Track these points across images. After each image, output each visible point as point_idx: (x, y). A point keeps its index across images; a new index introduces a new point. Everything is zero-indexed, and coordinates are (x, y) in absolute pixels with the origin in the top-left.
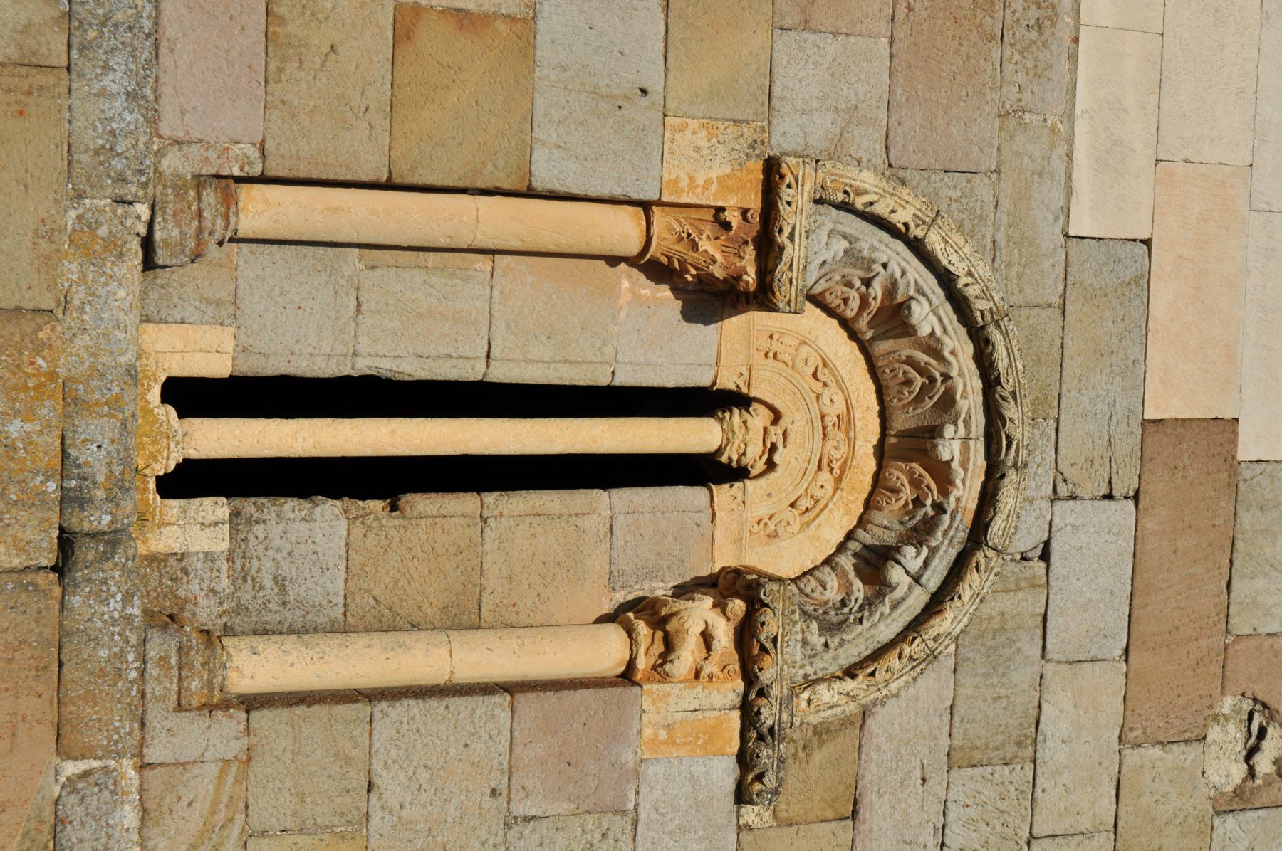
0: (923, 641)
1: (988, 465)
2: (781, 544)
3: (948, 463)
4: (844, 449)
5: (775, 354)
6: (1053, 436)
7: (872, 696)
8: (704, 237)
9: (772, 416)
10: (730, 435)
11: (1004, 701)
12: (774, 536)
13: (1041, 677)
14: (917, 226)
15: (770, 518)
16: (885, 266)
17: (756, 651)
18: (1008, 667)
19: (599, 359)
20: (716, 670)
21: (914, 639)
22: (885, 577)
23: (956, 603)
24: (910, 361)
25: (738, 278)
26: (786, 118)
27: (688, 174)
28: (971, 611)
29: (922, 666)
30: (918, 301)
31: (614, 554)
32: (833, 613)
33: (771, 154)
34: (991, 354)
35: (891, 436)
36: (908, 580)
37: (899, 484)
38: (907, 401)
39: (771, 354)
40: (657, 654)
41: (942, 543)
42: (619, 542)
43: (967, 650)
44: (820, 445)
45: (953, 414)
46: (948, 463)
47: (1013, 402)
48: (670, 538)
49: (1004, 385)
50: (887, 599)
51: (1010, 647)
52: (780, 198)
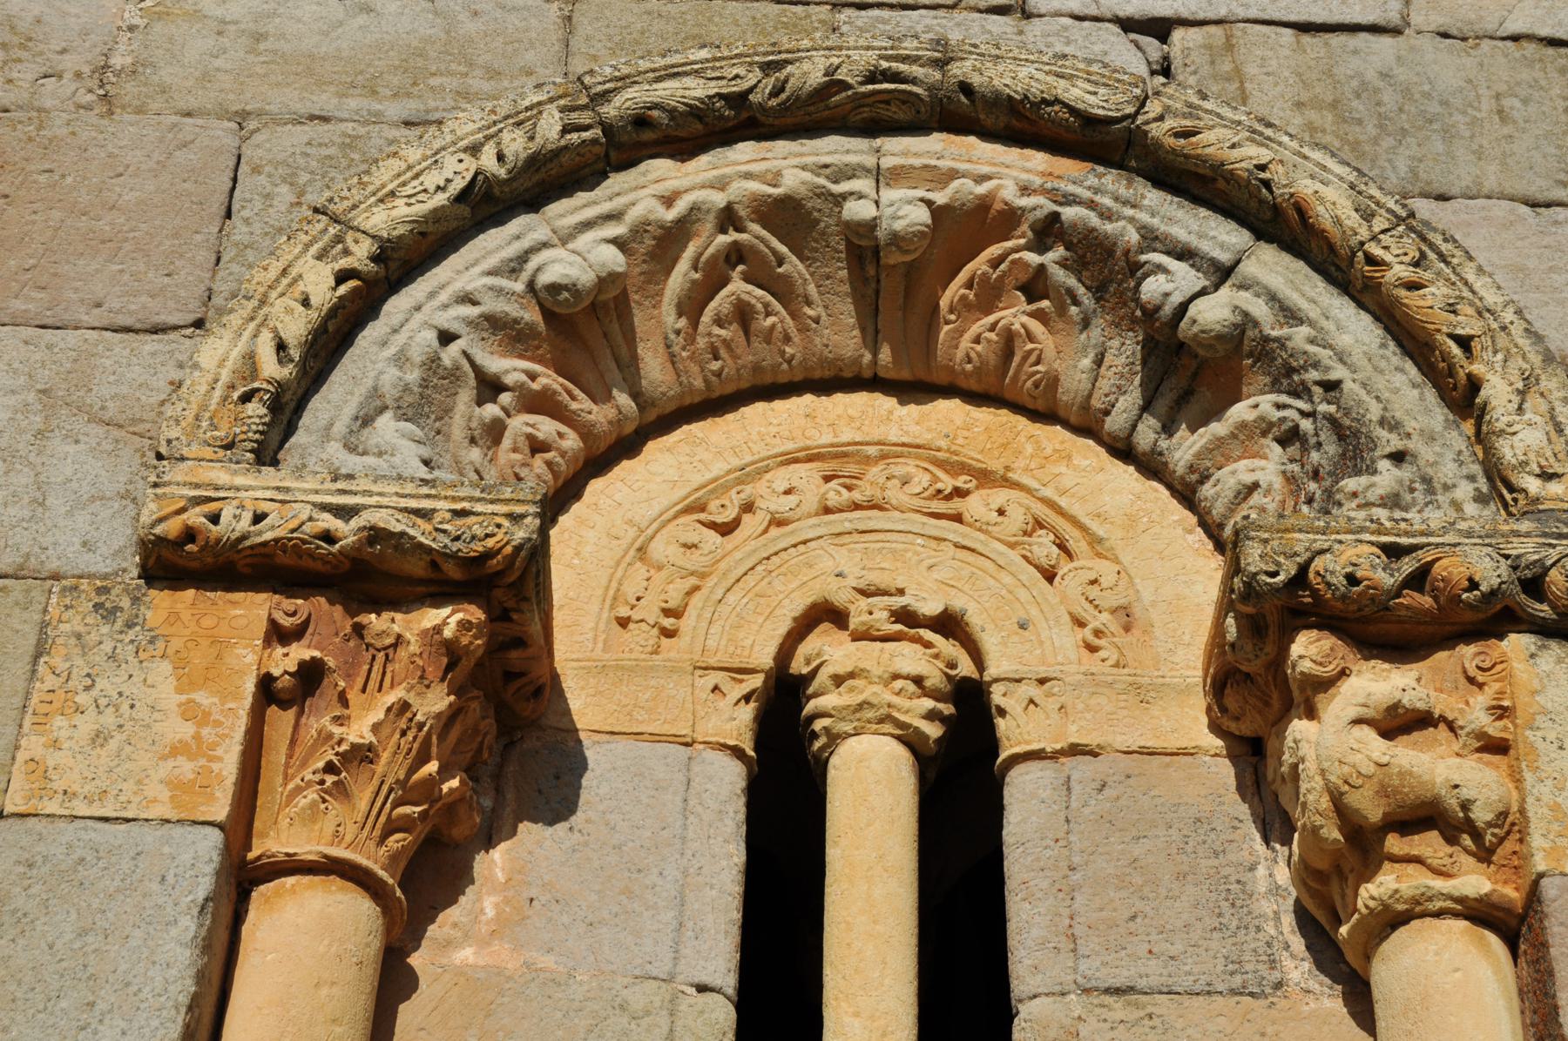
0: (1374, 238)
1: (941, 130)
2: (1147, 595)
3: (937, 212)
4: (907, 467)
5: (667, 612)
6: (876, 12)
7: (1521, 341)
8: (337, 730)
9: (825, 626)
10: (870, 714)
11: (1507, 102)
12: (1126, 616)
13: (1445, 35)
14: (346, 252)
15: (1081, 624)
16: (446, 338)
17: (1426, 601)
18: (1427, 96)
19: (664, 1022)
20: (1481, 700)
21: (1371, 260)
22: (1220, 337)
23: (1277, 174)
24: (692, 306)
25: (452, 653)
26: (47, 541)
27: (164, 758)
28: (1294, 144)
29: (1437, 239)
30: (538, 269)
31: (1186, 983)
32: (1315, 456)
33: (135, 572)
34: (672, 112)
35: (875, 361)
36: (1225, 291)
37: (992, 336)
38: (788, 319)
39: (668, 622)
40: (1449, 849)
41: (1132, 220)
42: (1152, 973)
43: (1389, 173)
44: (896, 514)
45: (818, 203)
46: (937, 212)
47: (789, 68)
48: (1137, 850)
49: (746, 85)
50: (1275, 333)
51: (1377, 91)
52: (244, 537)
